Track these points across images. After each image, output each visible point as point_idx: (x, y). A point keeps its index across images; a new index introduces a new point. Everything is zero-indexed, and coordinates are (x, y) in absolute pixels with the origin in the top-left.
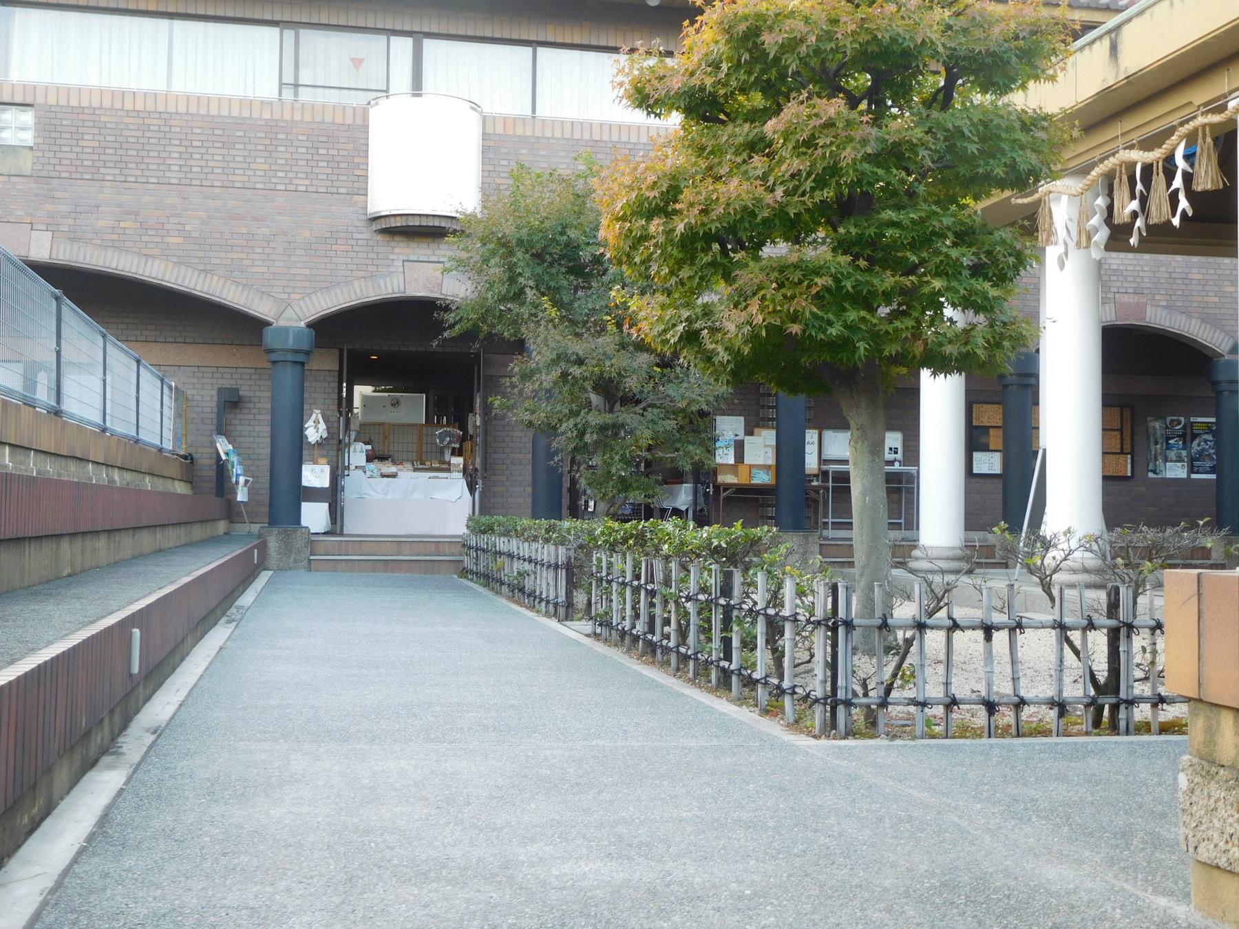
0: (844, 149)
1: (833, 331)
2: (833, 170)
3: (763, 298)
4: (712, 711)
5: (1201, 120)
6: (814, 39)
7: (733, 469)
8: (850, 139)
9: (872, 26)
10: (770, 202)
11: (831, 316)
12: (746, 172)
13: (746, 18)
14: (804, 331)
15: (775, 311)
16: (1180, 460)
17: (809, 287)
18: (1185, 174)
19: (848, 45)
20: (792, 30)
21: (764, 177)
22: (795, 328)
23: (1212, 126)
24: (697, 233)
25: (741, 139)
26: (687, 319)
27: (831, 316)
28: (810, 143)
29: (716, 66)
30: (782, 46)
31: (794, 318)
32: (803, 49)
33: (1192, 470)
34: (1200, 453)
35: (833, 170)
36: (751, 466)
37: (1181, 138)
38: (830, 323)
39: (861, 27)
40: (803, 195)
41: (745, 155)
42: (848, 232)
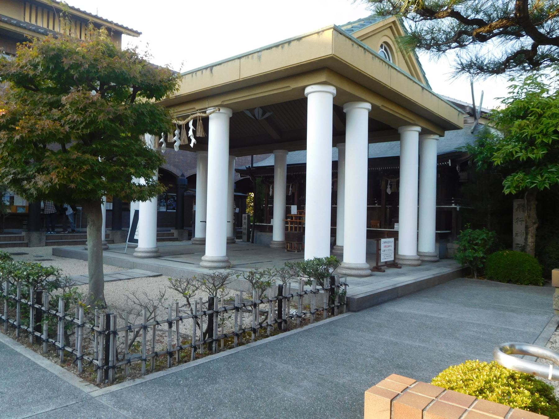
0: (100, 114)
1: (89, 187)
2: (93, 122)
3: (59, 172)
4: (37, 368)
5: (198, 114)
6: (87, 66)
7: (9, 207)
8: (102, 111)
9: (113, 66)
10: (63, 131)
11: (88, 180)
12: (49, 115)
13: (54, 50)
14: (76, 187)
15: (63, 178)
16: (164, 206)
17: (80, 169)
18: (193, 130)
19: (102, 71)
20: (78, 60)
21: (59, 119)
22: (73, 186)
23: (202, 117)
24: (26, 140)
25: (46, 101)
26: (14, 173)
27: (88, 180)
28: (85, 109)
29: (35, 66)
30: (71, 65)
31: (72, 182)
32: (82, 69)
33: (167, 209)
34: (170, 204)
35: (93, 122)
36: (17, 206)
37: (191, 119)
38: (88, 184)
39: (108, 65)
40: (78, 129)
41: (48, 108)
42: (97, 147)
